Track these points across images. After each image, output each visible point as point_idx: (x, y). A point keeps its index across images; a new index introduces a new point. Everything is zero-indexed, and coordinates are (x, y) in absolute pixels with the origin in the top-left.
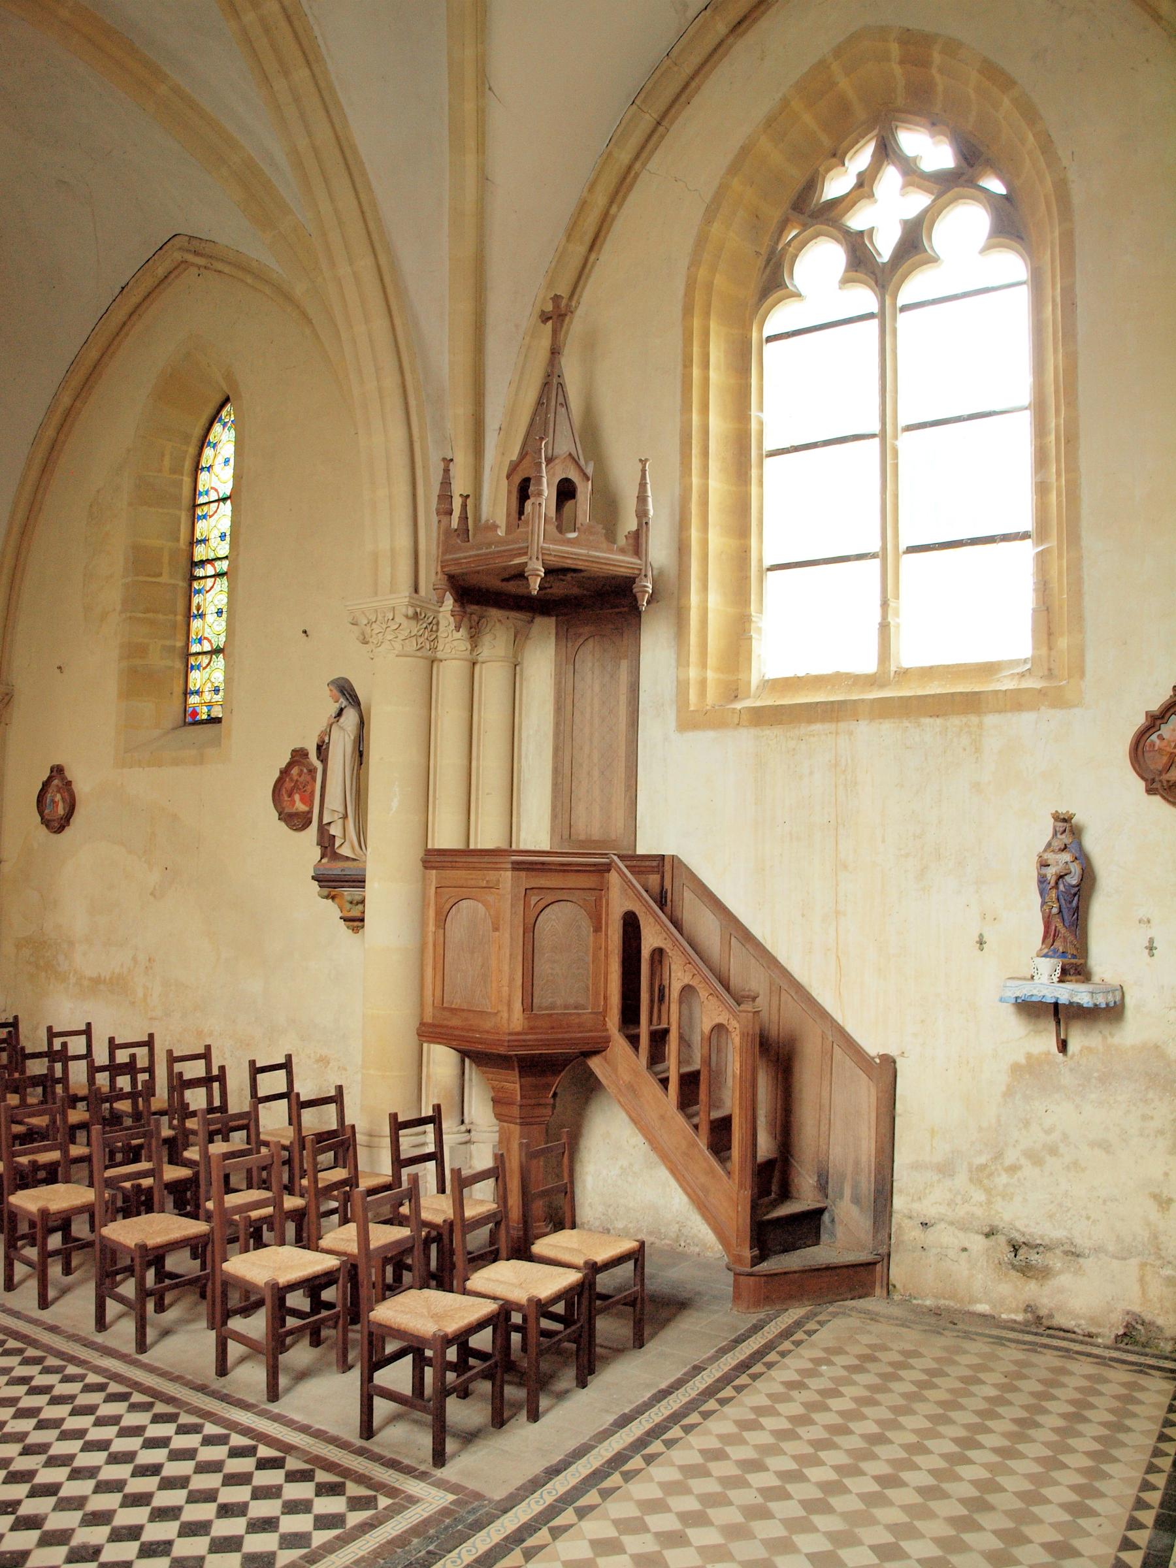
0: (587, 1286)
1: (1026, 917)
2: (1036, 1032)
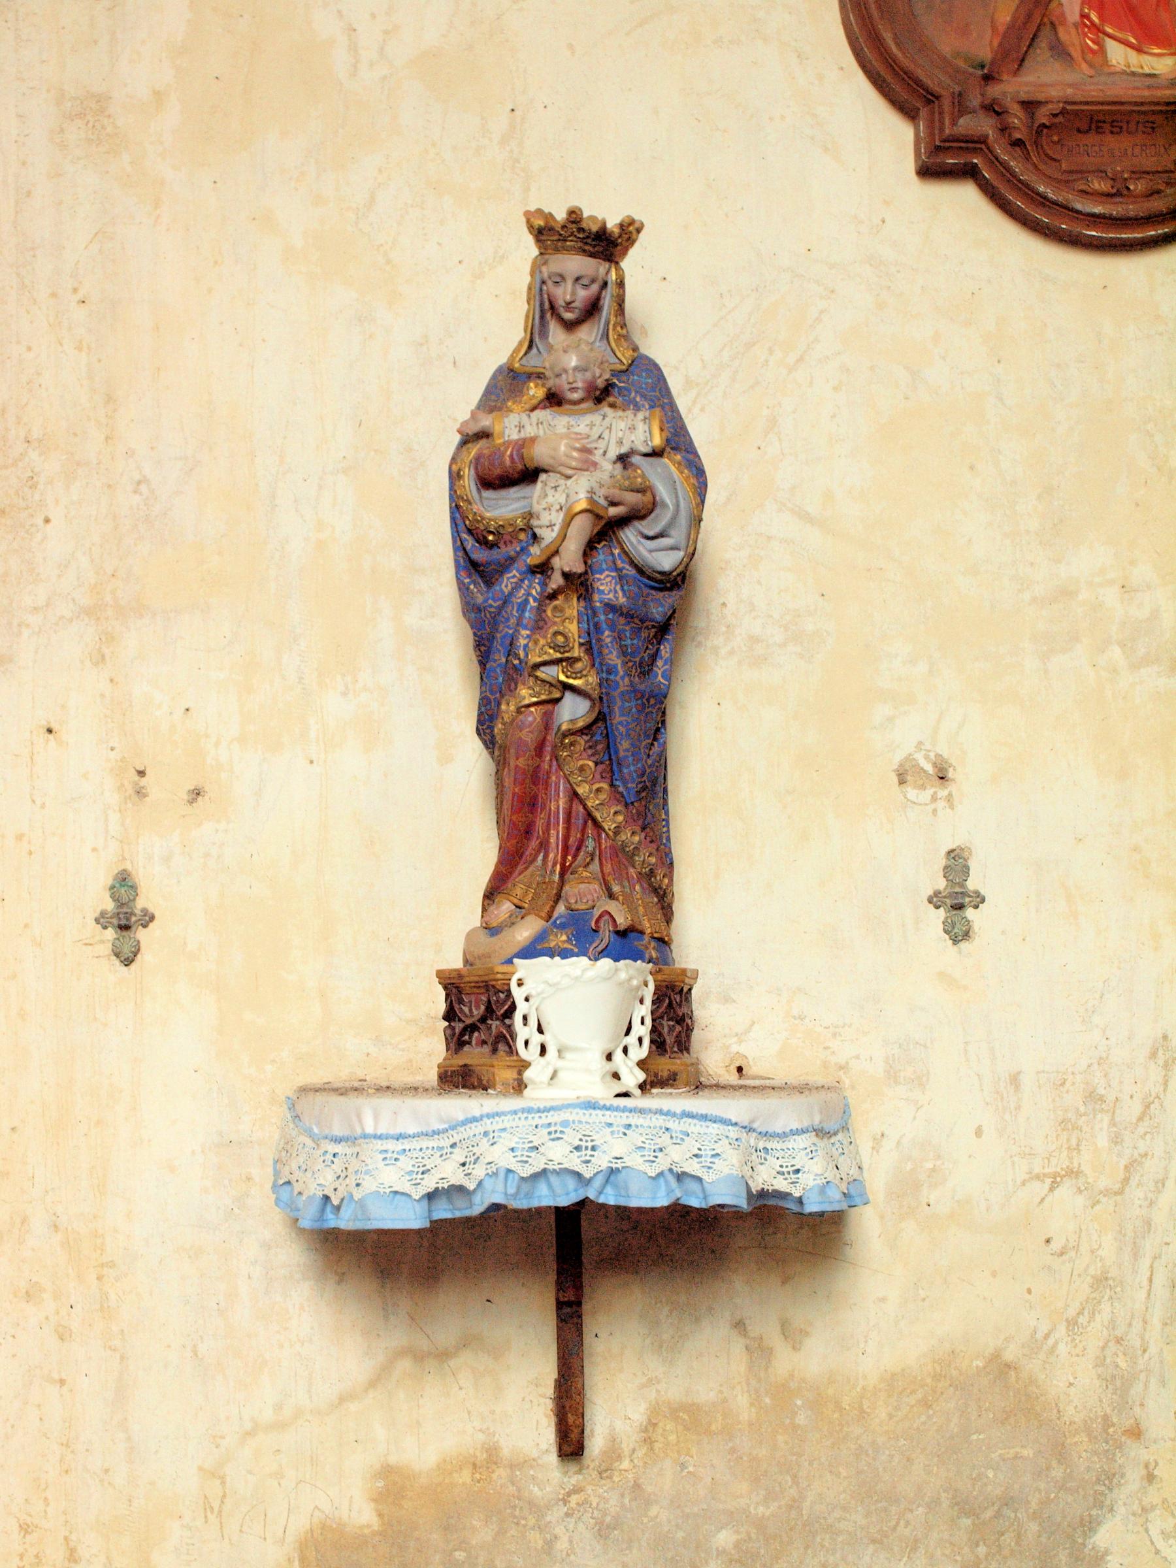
0: (470, 543)
1: (380, 787)
2: (419, 1357)
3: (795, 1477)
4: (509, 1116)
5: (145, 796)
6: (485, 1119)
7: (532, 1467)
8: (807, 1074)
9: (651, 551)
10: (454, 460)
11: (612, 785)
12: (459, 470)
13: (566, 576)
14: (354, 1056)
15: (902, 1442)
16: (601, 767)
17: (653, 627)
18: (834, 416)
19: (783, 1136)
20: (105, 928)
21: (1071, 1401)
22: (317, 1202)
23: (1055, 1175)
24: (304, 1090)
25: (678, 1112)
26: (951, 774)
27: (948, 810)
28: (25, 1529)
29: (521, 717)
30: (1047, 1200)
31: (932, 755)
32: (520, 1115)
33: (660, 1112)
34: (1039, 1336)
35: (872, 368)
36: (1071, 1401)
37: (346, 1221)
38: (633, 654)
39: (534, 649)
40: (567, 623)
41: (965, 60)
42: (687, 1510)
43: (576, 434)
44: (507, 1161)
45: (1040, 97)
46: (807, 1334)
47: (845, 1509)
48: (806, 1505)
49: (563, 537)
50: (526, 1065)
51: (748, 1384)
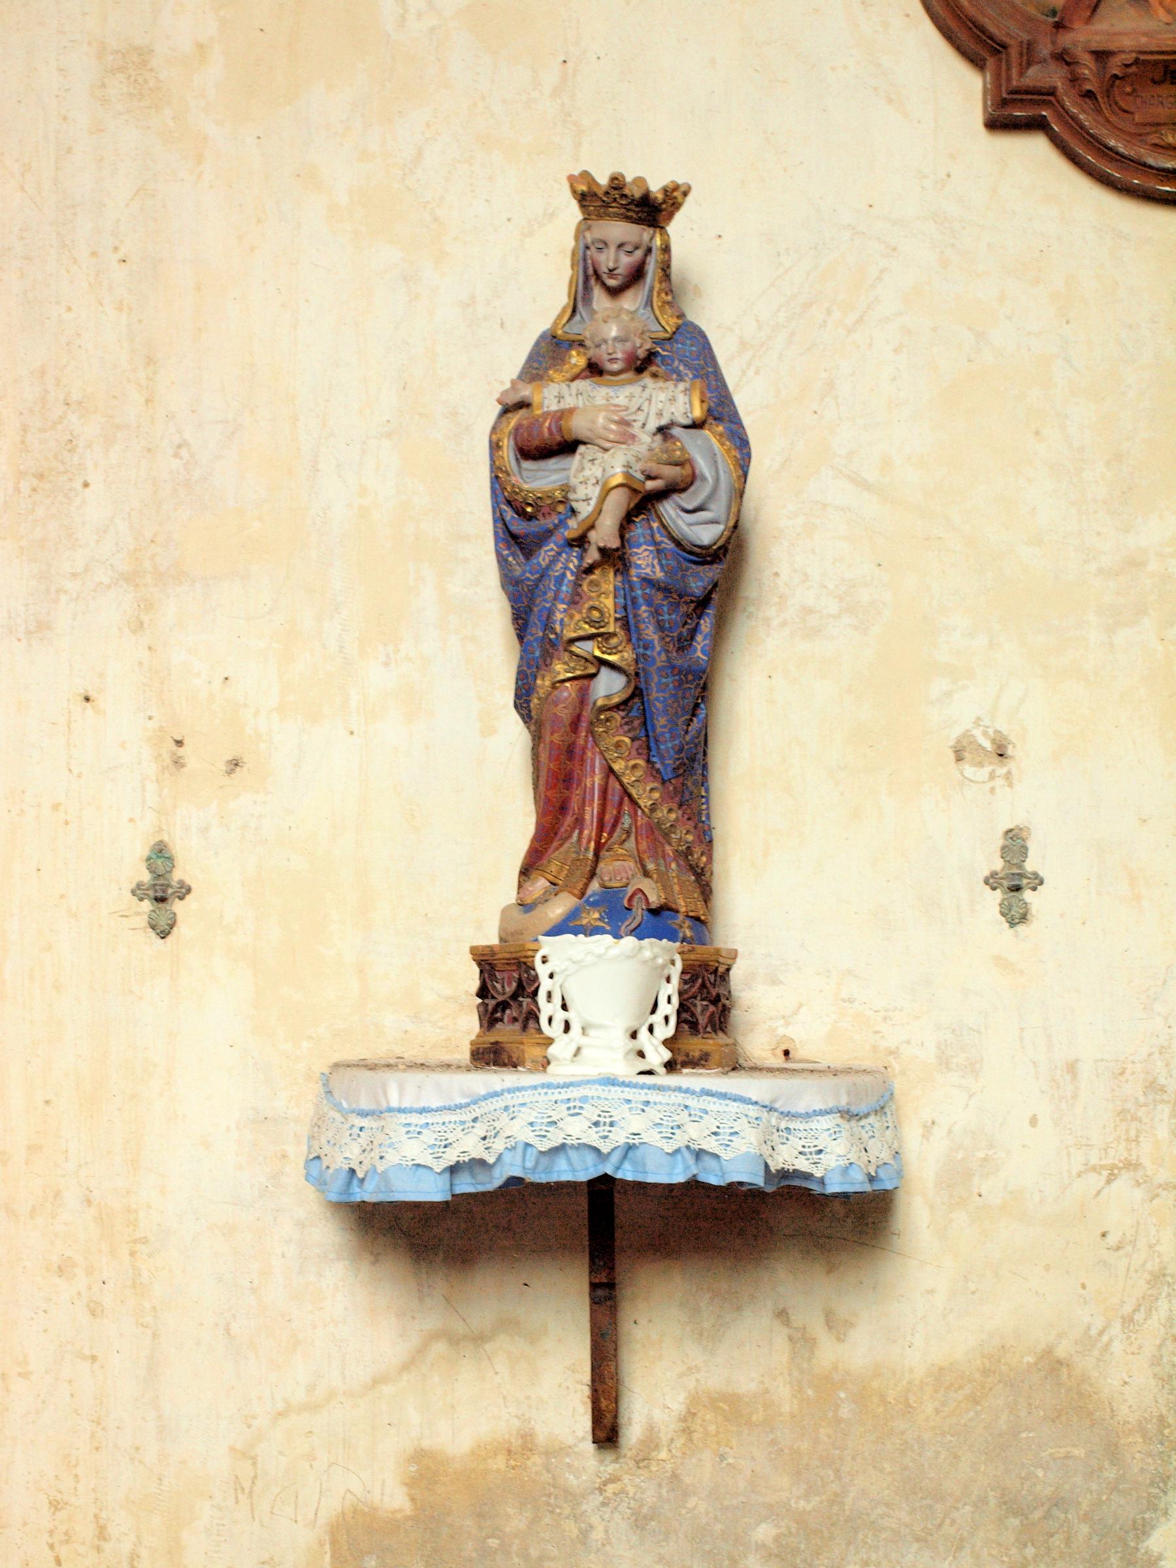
0: (509, 514)
1: (420, 756)
2: (454, 1341)
3: (837, 1471)
4: (529, 1092)
5: (183, 766)
6: (506, 1094)
7: (568, 1455)
8: (855, 1058)
9: (690, 525)
10: (494, 429)
11: (648, 761)
12: (499, 440)
13: (603, 551)
14: (391, 1032)
15: (949, 1438)
16: (637, 743)
17: (692, 602)
18: (894, 379)
19: (807, 1116)
20: (141, 900)
21: (1125, 1401)
22: (344, 1176)
23: (1112, 1167)
24: (337, 1066)
25: (698, 1089)
26: (1009, 751)
27: (1007, 789)
28: (56, 1506)
29: (556, 693)
30: (1103, 1194)
31: (991, 731)
32: (540, 1090)
33: (679, 1089)
34: (1094, 1332)
35: (934, 329)
36: (1125, 1401)
37: (369, 1193)
38: (671, 629)
39: (569, 623)
40: (602, 599)
41: (1037, 8)
42: (726, 1503)
43: (615, 405)
44: (528, 1136)
45: (1112, 47)
46: (852, 1325)
47: (887, 1505)
48: (848, 1500)
49: (599, 511)
50: (550, 1041)
51: (790, 1375)
